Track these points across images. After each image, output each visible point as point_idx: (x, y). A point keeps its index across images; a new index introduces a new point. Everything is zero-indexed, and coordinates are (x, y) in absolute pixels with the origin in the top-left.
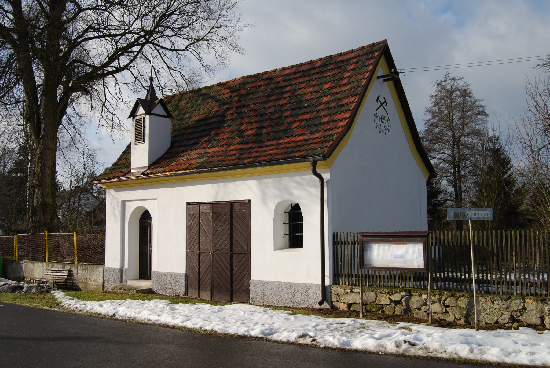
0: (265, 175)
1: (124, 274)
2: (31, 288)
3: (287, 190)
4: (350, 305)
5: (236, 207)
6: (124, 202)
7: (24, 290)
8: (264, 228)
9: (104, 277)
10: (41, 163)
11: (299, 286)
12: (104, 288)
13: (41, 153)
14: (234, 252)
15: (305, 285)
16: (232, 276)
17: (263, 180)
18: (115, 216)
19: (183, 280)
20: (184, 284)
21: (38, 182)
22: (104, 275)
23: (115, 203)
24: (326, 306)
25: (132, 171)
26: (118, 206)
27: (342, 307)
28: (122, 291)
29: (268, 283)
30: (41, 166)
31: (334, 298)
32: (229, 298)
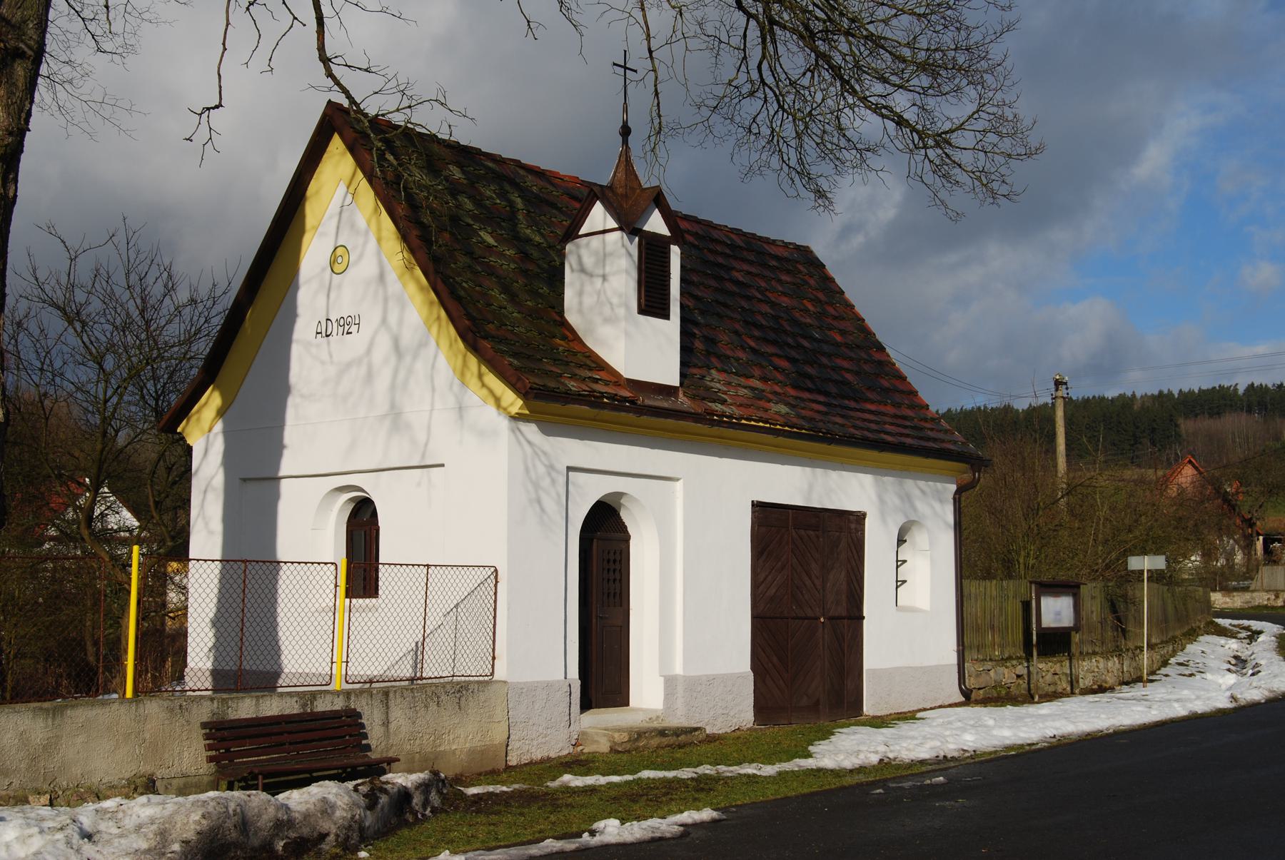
18: (543, 510)
26: (553, 481)
28: (665, 741)
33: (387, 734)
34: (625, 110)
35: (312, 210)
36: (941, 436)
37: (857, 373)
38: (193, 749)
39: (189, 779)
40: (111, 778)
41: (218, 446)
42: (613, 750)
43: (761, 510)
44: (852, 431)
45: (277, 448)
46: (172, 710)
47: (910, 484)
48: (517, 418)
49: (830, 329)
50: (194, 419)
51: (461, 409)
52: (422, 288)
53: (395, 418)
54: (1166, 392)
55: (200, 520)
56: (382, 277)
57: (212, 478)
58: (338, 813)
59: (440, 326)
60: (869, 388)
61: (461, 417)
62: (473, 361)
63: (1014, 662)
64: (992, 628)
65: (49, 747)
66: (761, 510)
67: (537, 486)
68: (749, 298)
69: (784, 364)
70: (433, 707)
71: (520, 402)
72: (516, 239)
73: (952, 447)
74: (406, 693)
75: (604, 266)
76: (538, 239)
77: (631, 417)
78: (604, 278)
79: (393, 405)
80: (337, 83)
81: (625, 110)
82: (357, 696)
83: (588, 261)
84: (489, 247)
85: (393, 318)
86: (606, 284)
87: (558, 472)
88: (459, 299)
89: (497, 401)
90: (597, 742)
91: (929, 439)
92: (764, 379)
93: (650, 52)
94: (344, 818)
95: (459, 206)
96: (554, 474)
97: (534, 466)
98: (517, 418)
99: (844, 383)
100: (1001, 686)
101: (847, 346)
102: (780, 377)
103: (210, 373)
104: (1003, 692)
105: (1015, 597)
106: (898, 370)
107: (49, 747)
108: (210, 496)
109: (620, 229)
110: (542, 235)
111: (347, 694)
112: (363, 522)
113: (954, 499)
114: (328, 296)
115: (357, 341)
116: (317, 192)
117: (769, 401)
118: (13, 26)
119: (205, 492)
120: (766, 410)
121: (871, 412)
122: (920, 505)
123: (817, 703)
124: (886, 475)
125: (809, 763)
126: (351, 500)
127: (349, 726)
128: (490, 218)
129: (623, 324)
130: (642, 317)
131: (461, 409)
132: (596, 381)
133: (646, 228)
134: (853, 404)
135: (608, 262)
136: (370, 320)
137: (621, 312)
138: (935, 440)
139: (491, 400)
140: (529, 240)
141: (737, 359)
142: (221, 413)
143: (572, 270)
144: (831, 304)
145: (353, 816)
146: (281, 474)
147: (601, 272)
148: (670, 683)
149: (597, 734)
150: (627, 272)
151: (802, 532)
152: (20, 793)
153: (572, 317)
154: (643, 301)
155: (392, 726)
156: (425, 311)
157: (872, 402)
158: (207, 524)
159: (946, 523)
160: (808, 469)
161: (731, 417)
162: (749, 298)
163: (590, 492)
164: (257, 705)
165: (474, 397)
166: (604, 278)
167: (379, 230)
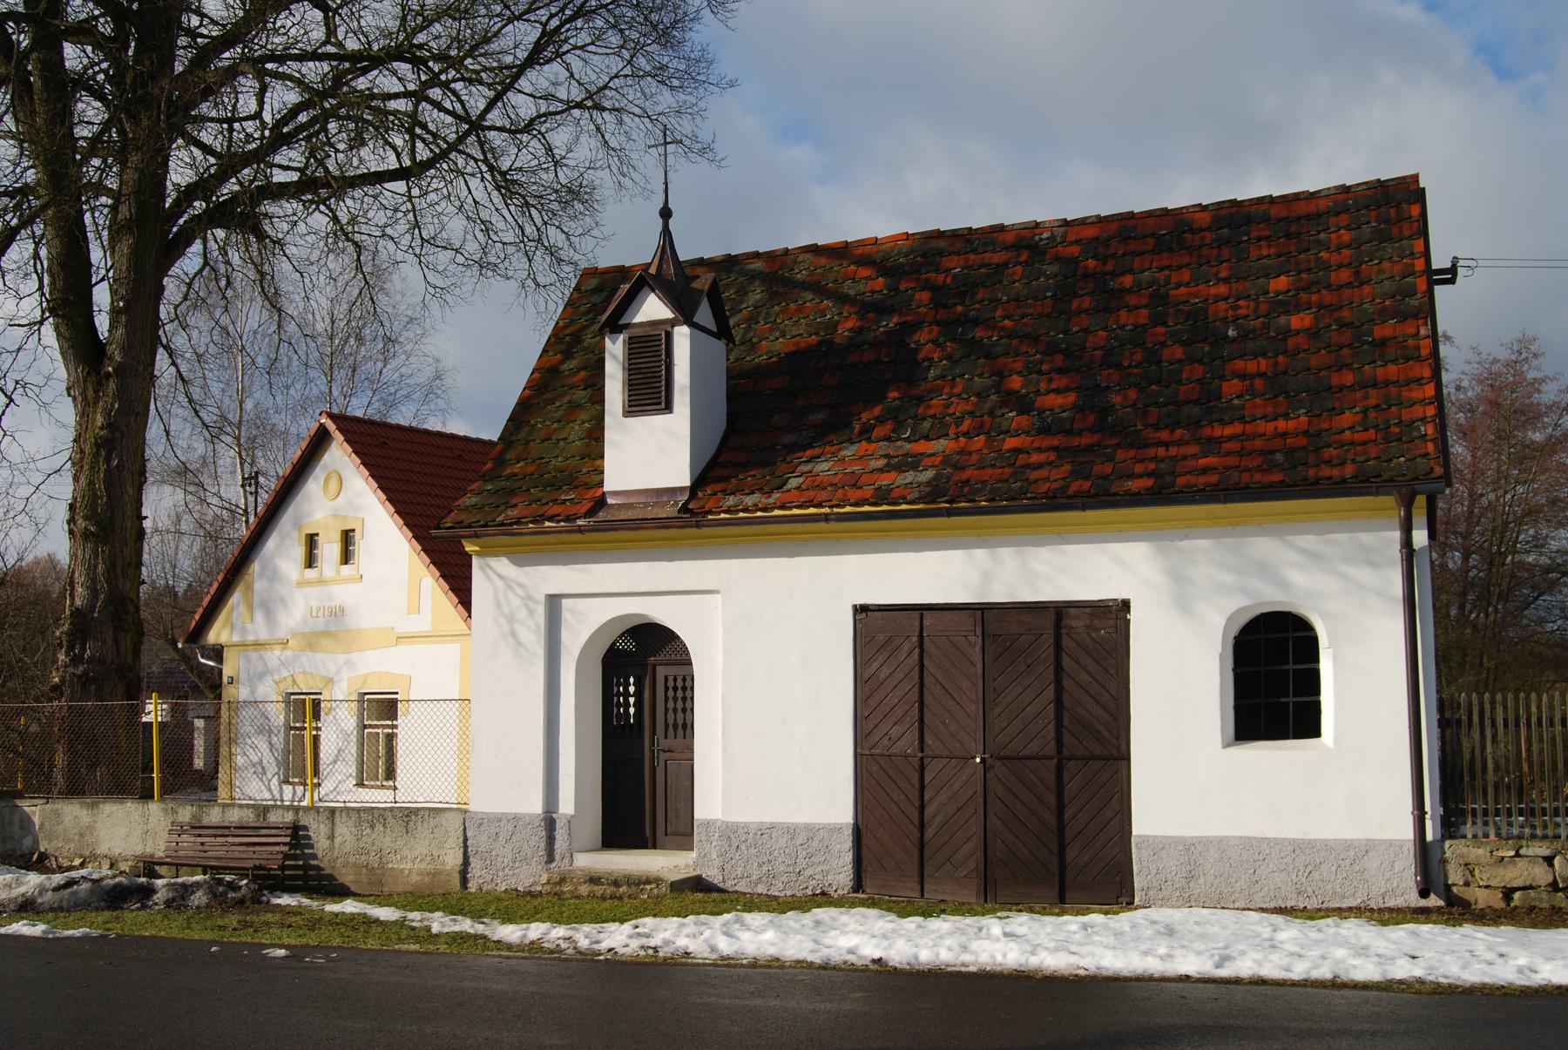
0: (1188, 529)
1: (560, 834)
2: (187, 889)
3: (1264, 570)
4: (1508, 893)
5: (1077, 623)
6: (554, 603)
7: (160, 896)
8: (1175, 686)
9: (466, 847)
10: (108, 460)
11: (1327, 846)
12: (464, 881)
13: (109, 425)
14: (927, 752)
15: (1349, 844)
16: (1061, 827)
17: (1178, 544)
18: (519, 643)
19: (847, 842)
20: (848, 857)
21: (97, 524)
22: (466, 840)
23: (516, 602)
24: (1434, 901)
25: (610, 501)
26: (531, 613)
27: (1481, 898)
28: (599, 890)
29: (1206, 842)
30: (108, 471)
31: (1455, 876)
32: (1055, 893)
33: (332, 847)
67: (511, 619)
70: (379, 827)
87: (536, 602)
96: (531, 605)
130: (632, 421)
155: (338, 840)
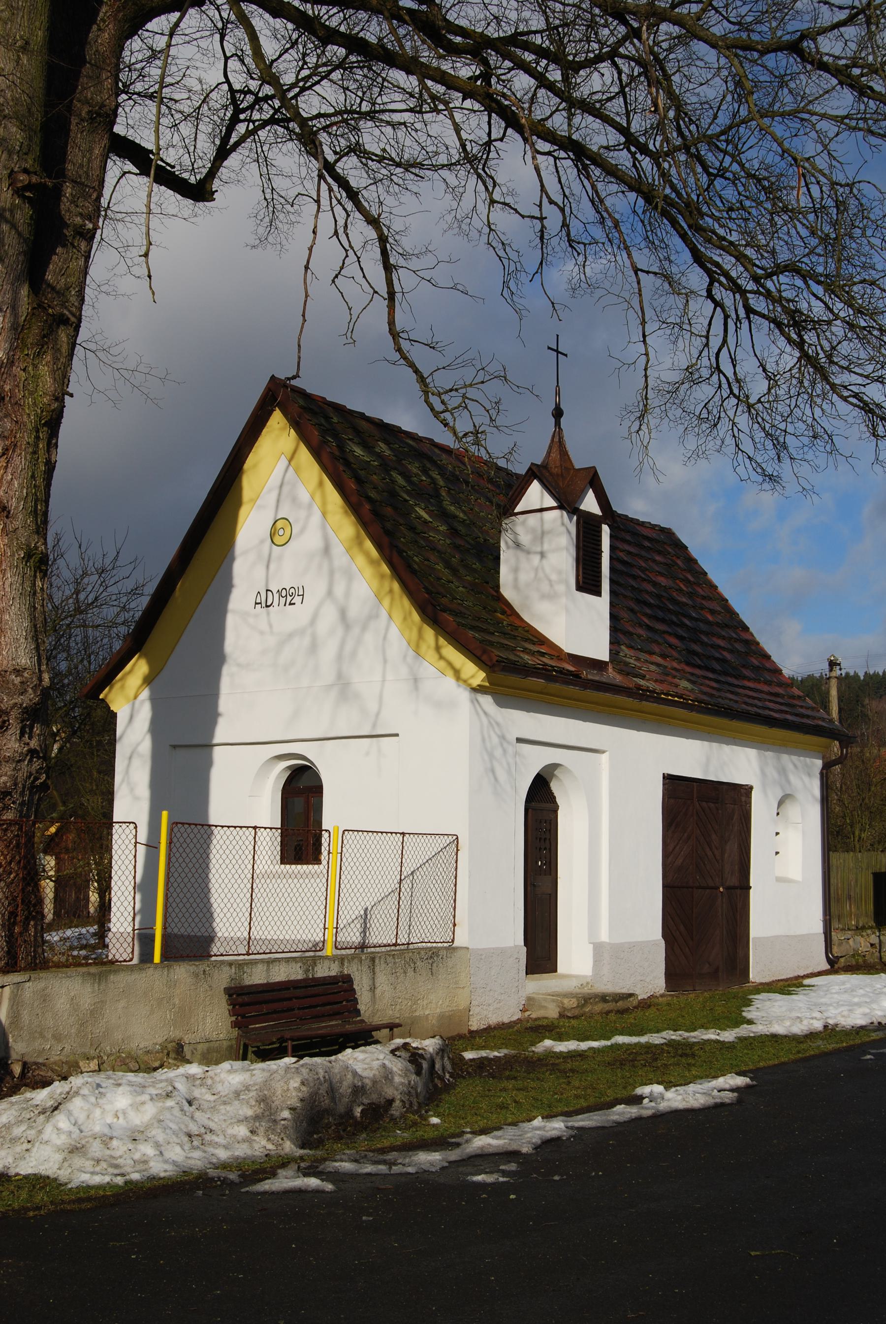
18: (496, 779)
28: (607, 1007)
34: (558, 393)
35: (249, 483)
36: (809, 713)
37: (731, 651)
38: (214, 1014)
39: (212, 1044)
40: (147, 1044)
41: (145, 713)
42: (562, 1015)
43: (671, 781)
44: (744, 706)
45: (211, 716)
46: (196, 975)
47: (785, 758)
48: (479, 690)
49: (702, 609)
50: (117, 686)
51: (416, 681)
52: (372, 562)
53: (343, 688)
54: (852, 674)
55: (124, 786)
56: (327, 550)
57: (138, 744)
58: (397, 1079)
59: (392, 599)
60: (744, 666)
61: (416, 688)
62: (429, 633)
63: (869, 931)
64: (849, 897)
65: (95, 1012)
66: (671, 781)
67: (491, 756)
68: (635, 577)
69: (673, 640)
70: (410, 973)
71: (482, 675)
72: (444, 515)
73: (820, 723)
74: (389, 959)
75: (542, 543)
76: (461, 515)
77: (572, 690)
78: (542, 555)
79: (340, 675)
80: (405, 358)
81: (558, 393)
82: (349, 962)
83: (525, 538)
84: (426, 522)
85: (339, 590)
86: (544, 561)
87: (509, 743)
88: (414, 572)
89: (457, 673)
90: (545, 1008)
91: (803, 716)
92: (664, 656)
93: (644, 336)
94: (402, 1084)
95: (393, 481)
96: (505, 745)
97: (490, 737)
98: (479, 690)
99: (724, 661)
100: (859, 955)
101: (718, 624)
102: (675, 654)
103: (138, 641)
104: (861, 960)
105: (867, 869)
106: (762, 649)
107: (95, 1012)
108: (136, 762)
109: (560, 507)
110: (464, 512)
111: (342, 960)
112: (302, 790)
113: (821, 774)
114: (268, 567)
115: (300, 613)
116: (255, 466)
117: (675, 677)
118: (58, 293)
119: (130, 758)
120: (677, 686)
121: (751, 689)
122: (793, 778)
123: (717, 970)
124: (768, 750)
125: (744, 1031)
126: (289, 767)
127: (345, 991)
128: (419, 494)
129: (564, 600)
131: (416, 681)
132: (543, 654)
133: (582, 507)
134: (736, 682)
135: (546, 540)
136: (316, 590)
137: (561, 588)
138: (808, 717)
139: (450, 673)
140: (455, 517)
141: (639, 636)
142: (148, 680)
143: (508, 547)
144: (699, 585)
145: (410, 1082)
146: (216, 741)
147: (539, 549)
148: (598, 949)
149: (545, 1000)
150: (567, 549)
151: (704, 804)
152: (72, 1058)
153: (507, 591)
154: (581, 578)
155: (378, 992)
156: (375, 583)
157: (749, 679)
158: (132, 790)
159: (813, 796)
160: (706, 743)
161: (654, 691)
162: (635, 577)
163: (536, 761)
164: (268, 970)
165: (429, 669)
166: (542, 555)
167: (324, 503)
